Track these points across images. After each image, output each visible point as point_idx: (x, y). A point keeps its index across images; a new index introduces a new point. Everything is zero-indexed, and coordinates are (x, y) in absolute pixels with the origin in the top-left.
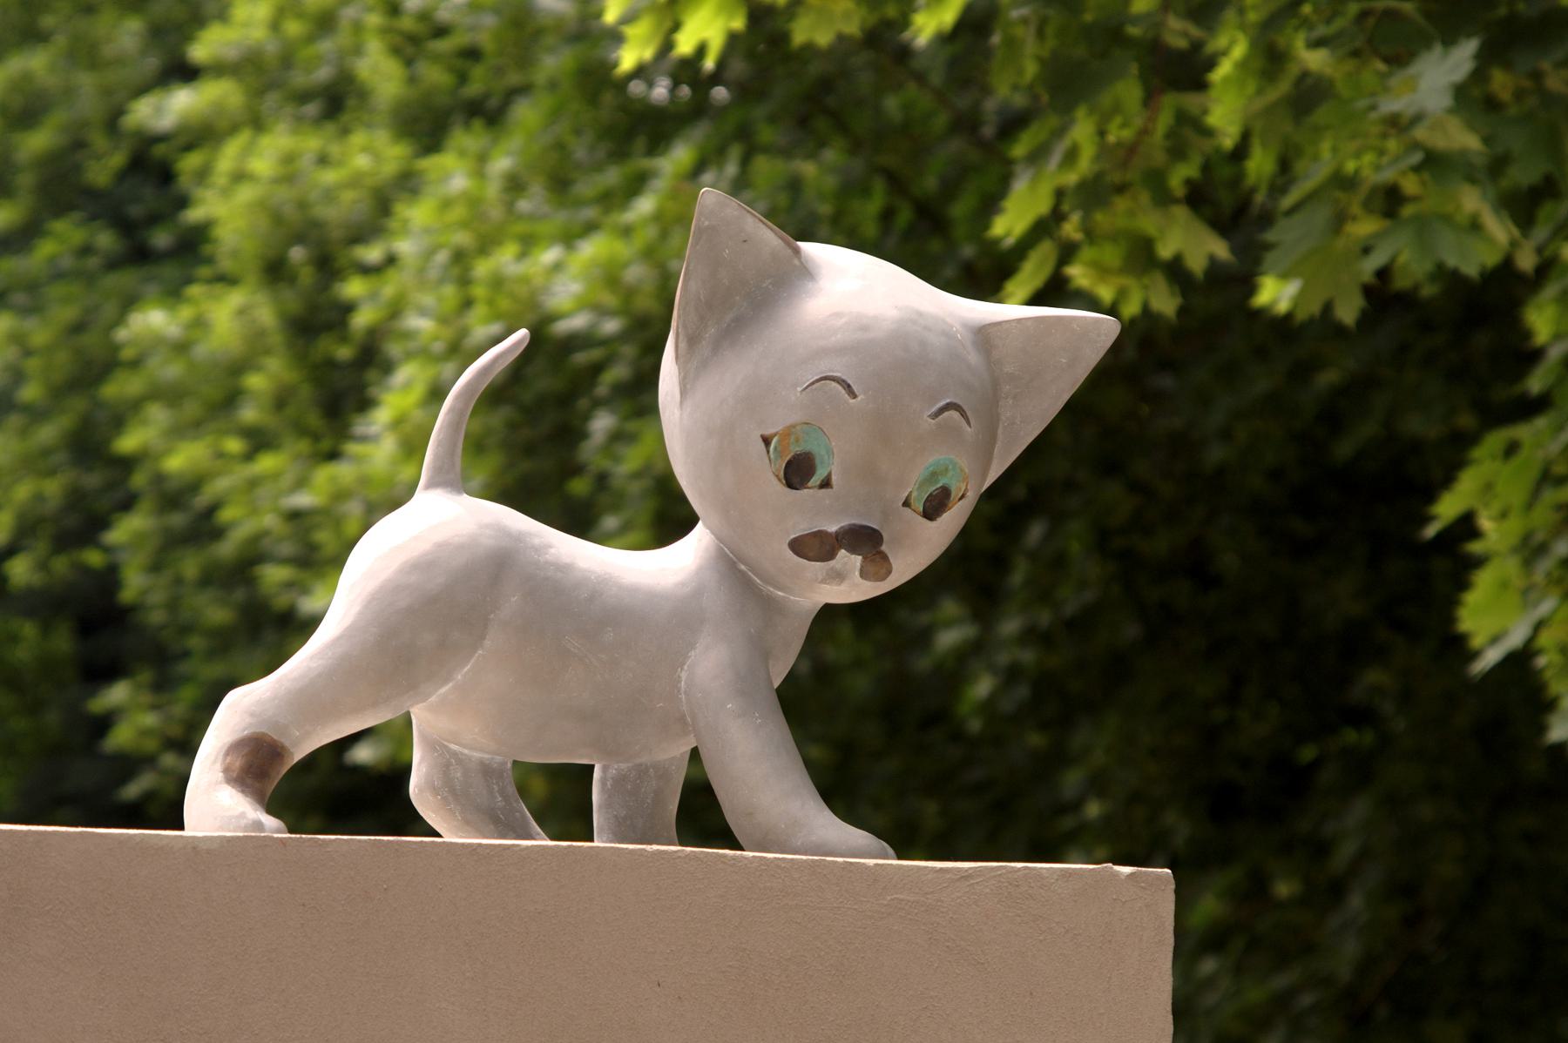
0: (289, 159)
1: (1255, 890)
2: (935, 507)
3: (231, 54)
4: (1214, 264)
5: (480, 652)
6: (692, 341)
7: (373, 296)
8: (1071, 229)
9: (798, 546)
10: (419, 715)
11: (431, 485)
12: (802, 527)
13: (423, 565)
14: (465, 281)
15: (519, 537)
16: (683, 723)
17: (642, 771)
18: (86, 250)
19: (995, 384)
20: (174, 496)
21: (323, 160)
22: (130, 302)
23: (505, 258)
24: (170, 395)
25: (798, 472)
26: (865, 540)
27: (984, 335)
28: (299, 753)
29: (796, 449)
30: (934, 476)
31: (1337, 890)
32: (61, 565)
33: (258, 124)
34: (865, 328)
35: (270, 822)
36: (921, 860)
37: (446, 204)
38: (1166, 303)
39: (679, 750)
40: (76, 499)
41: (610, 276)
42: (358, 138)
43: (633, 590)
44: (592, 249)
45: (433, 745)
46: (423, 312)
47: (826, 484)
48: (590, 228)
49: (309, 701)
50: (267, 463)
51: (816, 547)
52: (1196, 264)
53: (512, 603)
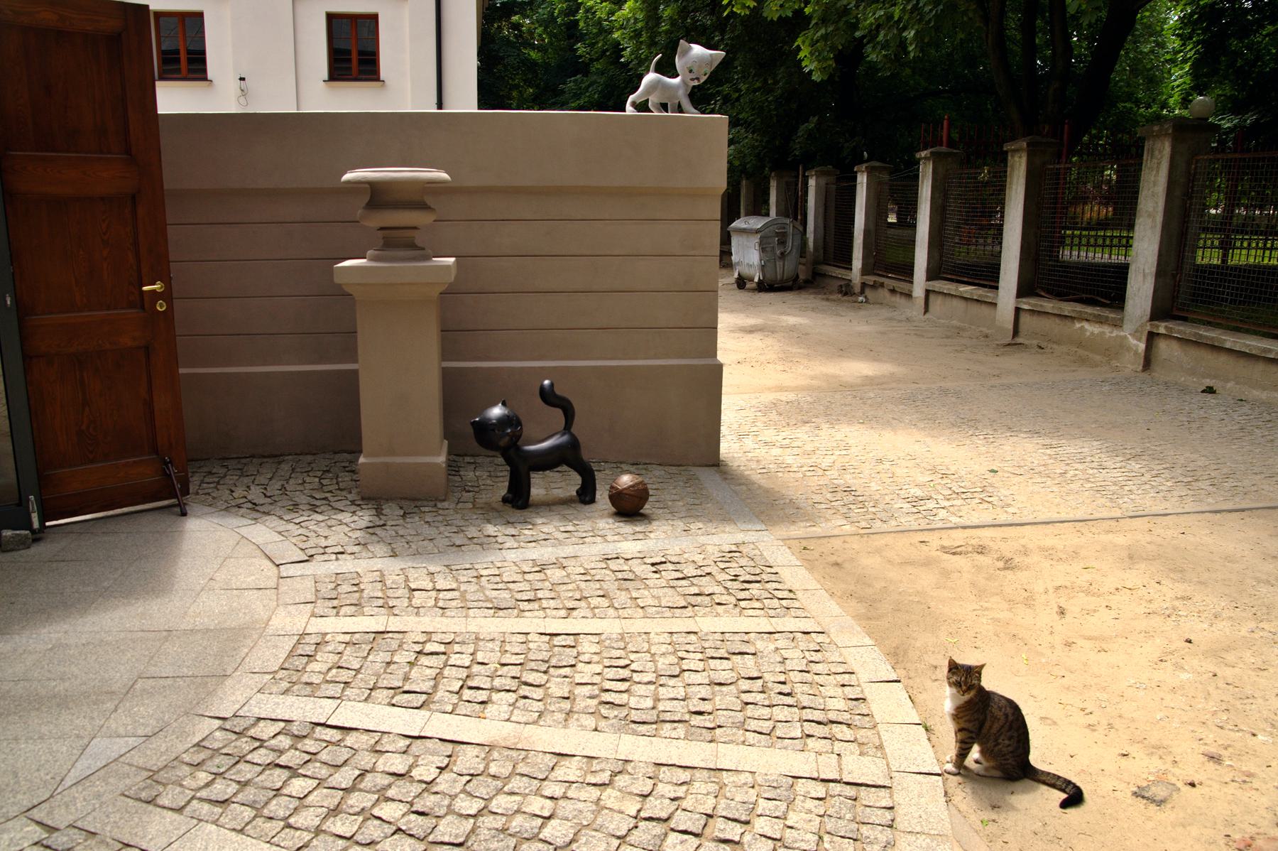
1: (765, 81)
4: (754, 6)
5: (921, 479)
6: (679, 57)
26: (698, 79)
27: (711, 55)
31: (778, 82)
36: (643, 366)
38: (748, 13)
39: (677, 101)
49: (639, 97)
51: (692, 80)
52: (752, 6)
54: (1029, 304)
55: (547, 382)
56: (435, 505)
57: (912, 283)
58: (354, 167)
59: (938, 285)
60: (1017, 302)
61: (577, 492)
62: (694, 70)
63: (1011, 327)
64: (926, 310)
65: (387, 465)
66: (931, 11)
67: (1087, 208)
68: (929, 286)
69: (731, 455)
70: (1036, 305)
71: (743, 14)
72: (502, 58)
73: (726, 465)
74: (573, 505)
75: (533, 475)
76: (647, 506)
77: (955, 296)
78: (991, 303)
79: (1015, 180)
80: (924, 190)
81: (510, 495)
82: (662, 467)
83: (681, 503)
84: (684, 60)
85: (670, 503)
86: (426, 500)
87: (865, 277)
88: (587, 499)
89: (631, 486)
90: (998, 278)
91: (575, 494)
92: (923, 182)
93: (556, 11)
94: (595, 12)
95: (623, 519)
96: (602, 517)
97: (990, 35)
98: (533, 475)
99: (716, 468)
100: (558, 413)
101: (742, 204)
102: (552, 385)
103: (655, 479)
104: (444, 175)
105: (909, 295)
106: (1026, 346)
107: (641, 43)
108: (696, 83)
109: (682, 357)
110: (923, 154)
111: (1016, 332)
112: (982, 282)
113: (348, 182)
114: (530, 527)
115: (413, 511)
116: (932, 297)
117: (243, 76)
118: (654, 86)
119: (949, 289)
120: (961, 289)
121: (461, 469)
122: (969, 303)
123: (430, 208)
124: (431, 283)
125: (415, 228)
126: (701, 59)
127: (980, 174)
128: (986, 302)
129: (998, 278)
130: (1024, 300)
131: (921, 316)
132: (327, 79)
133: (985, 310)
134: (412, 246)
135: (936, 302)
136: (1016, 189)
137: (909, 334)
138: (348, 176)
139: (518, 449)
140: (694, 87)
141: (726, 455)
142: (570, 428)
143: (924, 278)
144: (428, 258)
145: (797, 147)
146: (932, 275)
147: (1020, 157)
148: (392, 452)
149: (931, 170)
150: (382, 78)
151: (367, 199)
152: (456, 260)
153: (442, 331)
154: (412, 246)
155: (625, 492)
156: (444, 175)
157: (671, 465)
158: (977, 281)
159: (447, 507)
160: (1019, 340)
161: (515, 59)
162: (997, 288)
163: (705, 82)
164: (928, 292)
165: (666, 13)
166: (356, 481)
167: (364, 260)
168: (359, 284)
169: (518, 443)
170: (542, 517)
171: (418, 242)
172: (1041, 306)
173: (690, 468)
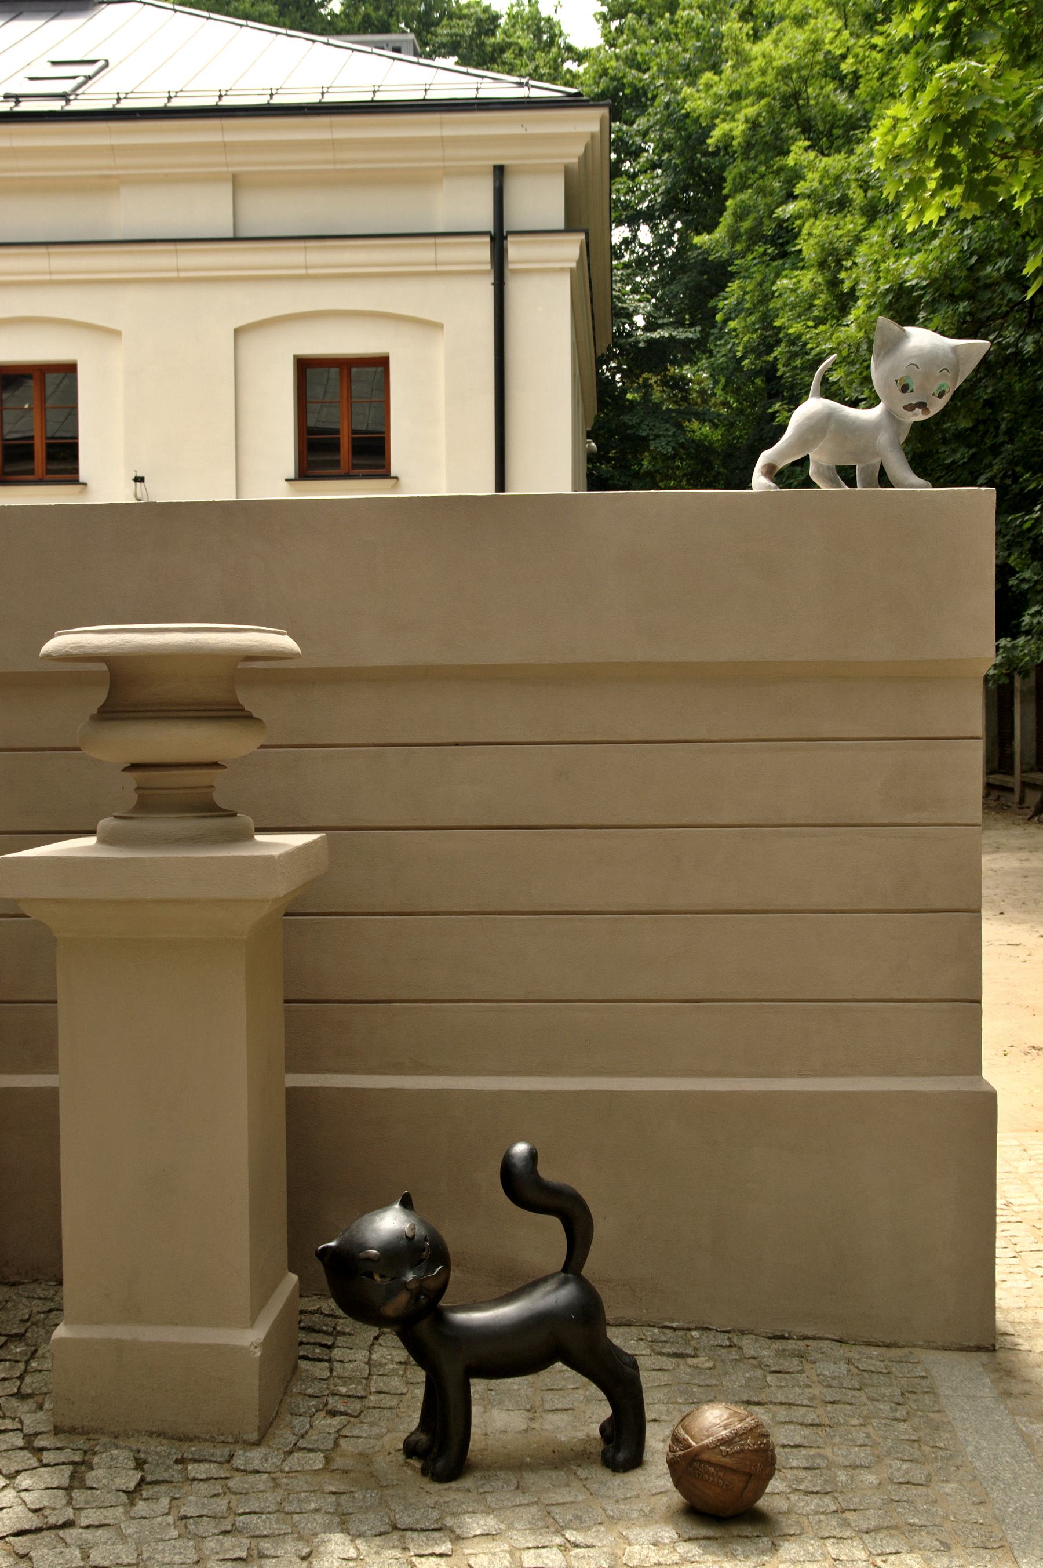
0: (826, 228)
2: (941, 395)
3: (808, 192)
6: (878, 356)
7: (849, 277)
9: (905, 408)
10: (811, 455)
11: (812, 396)
12: (906, 403)
13: (809, 418)
14: (878, 271)
15: (834, 409)
16: (878, 454)
17: (868, 466)
18: (765, 253)
19: (958, 361)
20: (793, 341)
21: (837, 227)
22: (778, 275)
23: (890, 263)
25: (905, 389)
26: (922, 405)
27: (955, 349)
28: (780, 467)
29: (903, 383)
30: (940, 387)
32: (924, 99)
33: (816, 215)
34: (922, 350)
35: (773, 485)
37: (872, 246)
39: (876, 461)
40: (763, 339)
41: (924, 267)
42: (849, 218)
43: (864, 421)
44: (919, 258)
45: (815, 462)
46: (864, 282)
47: (912, 391)
48: (919, 250)
49: (782, 454)
50: (821, 328)
51: (910, 408)
53: (832, 426)
55: (521, 1148)
61: (602, 1430)
62: (913, 386)
65: (119, 1347)
69: (1029, 1315)
72: (645, 440)
73: (1013, 1349)
74: (582, 1473)
75: (478, 1387)
76: (775, 1485)
81: (423, 1437)
82: (841, 1350)
83: (871, 1478)
84: (888, 364)
85: (842, 1477)
86: (212, 1440)
88: (621, 1456)
89: (724, 1442)
91: (597, 1433)
93: (740, 348)
95: (704, 1532)
96: (648, 1518)
98: (478, 1387)
99: (984, 1357)
100: (554, 1225)
101: (192, 855)
102: (533, 1156)
103: (816, 1390)
104: (285, 642)
108: (919, 416)
109: (892, 1072)
114: (445, 1547)
115: (166, 1476)
117: (139, 475)
118: (819, 427)
121: (341, 1340)
123: (249, 717)
124: (223, 900)
125: (215, 765)
126: (929, 360)
132: (292, 475)
138: (59, 643)
139: (439, 1317)
140: (917, 426)
141: (1016, 1316)
144: (243, 836)
145: (751, 156)
148: (133, 1314)
149: (106, 856)
150: (393, 473)
151: (100, 696)
152: (327, 835)
153: (286, 1002)
154: (209, 808)
155: (705, 1456)
156: (285, 642)
157: (869, 1344)
159: (256, 1464)
161: (668, 443)
163: (944, 413)
167: (91, 841)
168: (57, 901)
169: (442, 1304)
170: (489, 1511)
173: (919, 1354)
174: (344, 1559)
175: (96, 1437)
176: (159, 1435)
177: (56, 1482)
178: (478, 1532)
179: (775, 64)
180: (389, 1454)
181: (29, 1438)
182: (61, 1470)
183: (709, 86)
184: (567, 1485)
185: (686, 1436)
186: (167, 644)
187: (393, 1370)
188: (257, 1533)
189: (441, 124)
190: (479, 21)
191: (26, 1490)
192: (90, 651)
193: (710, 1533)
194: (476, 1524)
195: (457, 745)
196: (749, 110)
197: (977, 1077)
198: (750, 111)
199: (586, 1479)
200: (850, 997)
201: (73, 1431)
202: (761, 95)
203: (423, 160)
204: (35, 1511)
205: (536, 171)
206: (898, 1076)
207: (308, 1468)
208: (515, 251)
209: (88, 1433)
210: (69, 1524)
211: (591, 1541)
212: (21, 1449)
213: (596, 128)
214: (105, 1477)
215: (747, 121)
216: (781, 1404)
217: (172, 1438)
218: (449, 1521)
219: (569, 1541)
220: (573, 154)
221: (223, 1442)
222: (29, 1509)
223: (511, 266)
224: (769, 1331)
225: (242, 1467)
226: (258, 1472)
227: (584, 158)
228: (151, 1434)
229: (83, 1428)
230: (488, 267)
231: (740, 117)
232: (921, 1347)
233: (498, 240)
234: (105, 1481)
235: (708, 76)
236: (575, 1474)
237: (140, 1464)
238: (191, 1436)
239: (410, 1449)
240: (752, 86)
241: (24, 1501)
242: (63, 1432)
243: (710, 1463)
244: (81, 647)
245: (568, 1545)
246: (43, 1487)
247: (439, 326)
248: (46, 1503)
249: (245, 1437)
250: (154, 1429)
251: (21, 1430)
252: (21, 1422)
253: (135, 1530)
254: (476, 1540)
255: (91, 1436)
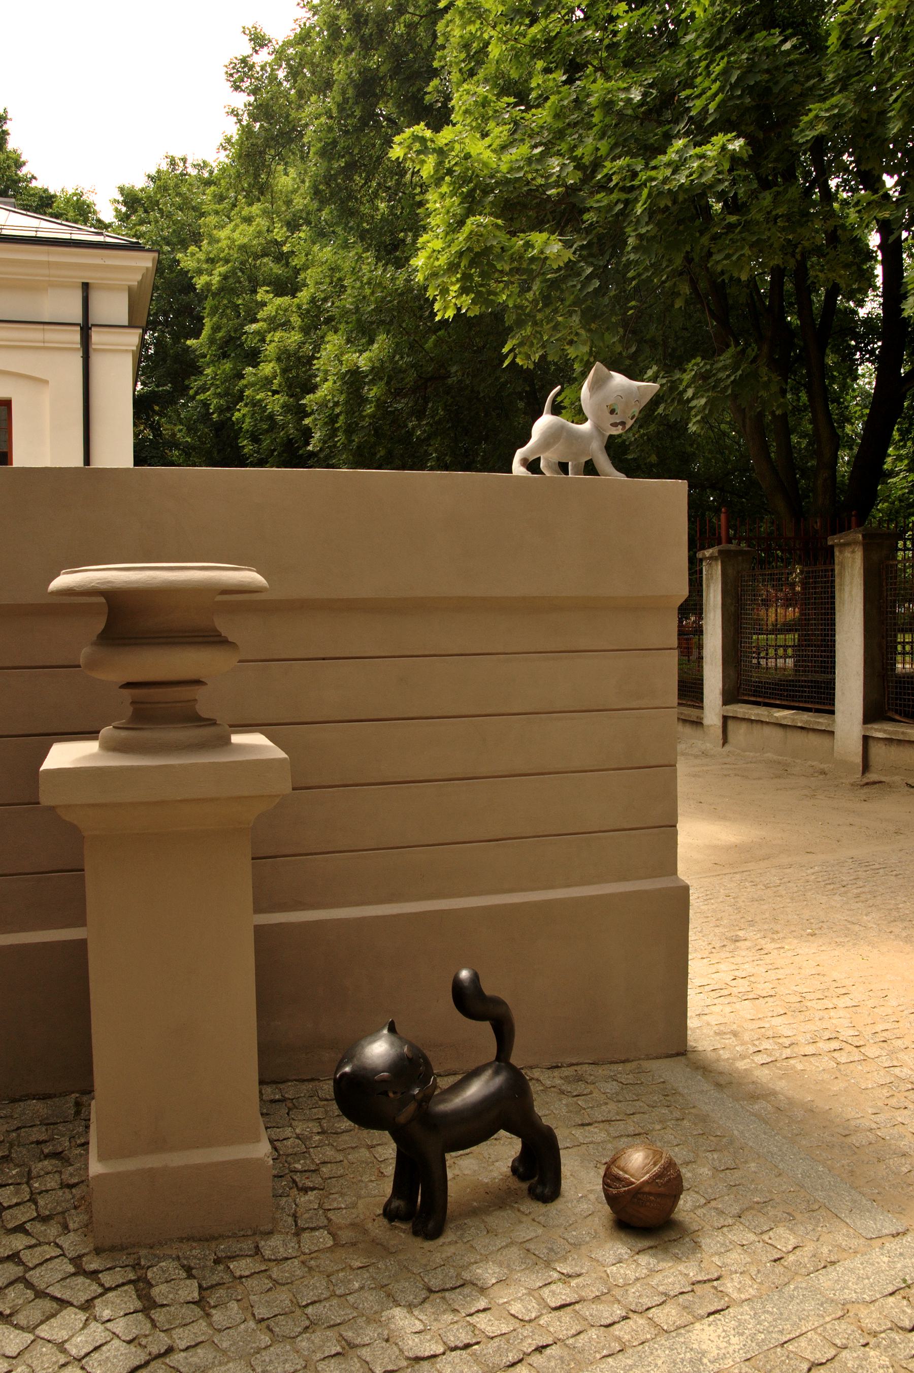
8: (517, 351)
9: (612, 425)
11: (547, 413)
12: (612, 422)
24: (253, 385)
44: (366, 355)
49: (532, 451)
51: (614, 425)
54: (885, 731)
55: (465, 974)
56: (257, 1250)
57: (702, 708)
58: (75, 563)
59: (740, 710)
60: (865, 729)
63: (858, 760)
64: (725, 741)
65: (151, 1174)
66: (729, 376)
67: (772, 611)
68: (727, 711)
70: (896, 732)
71: (525, 367)
75: (450, 1157)
77: (767, 723)
78: (828, 731)
79: (847, 579)
80: (712, 595)
87: (728, 707)
90: (834, 699)
92: (708, 586)
94: (266, 406)
95: (646, 1243)
97: (747, 421)
98: (450, 1157)
102: (475, 978)
104: (250, 576)
105: (698, 723)
106: (890, 785)
107: (337, 429)
109: (624, 879)
110: (708, 553)
111: (866, 766)
112: (801, 705)
113: (68, 592)
114: (482, 1304)
116: (731, 725)
119: (758, 715)
120: (777, 715)
122: (754, 724)
125: (198, 682)
127: (791, 574)
128: (814, 730)
129: (833, 695)
130: (876, 726)
131: (719, 749)
133: (814, 740)
134: (196, 719)
135: (739, 733)
136: (851, 592)
137: (729, 775)
138: (64, 580)
142: (508, 1055)
143: (719, 700)
146: (730, 696)
147: (853, 552)
148: (159, 1144)
151: (99, 625)
154: (196, 719)
157: (612, 1063)
158: (797, 704)
160: (872, 777)
162: (832, 712)
164: (725, 719)
165: (372, 394)
166: (71, 1186)
171: (204, 710)
172: (903, 733)
174: (416, 1333)
175: (135, 1250)
176: (188, 1240)
177: (132, 1307)
178: (494, 1281)
179: (236, 243)
180: (374, 1220)
181: (76, 1261)
182: (126, 1291)
183: (193, 254)
184: (520, 1222)
185: (627, 1176)
186: (189, 581)
187: (320, 1141)
188: (332, 1323)
189: (48, 253)
190: (41, 198)
191: (109, 1321)
192: (119, 586)
193: (652, 1243)
194: (488, 1273)
195: (324, 659)
196: (221, 269)
197: (673, 877)
198: (223, 269)
199: (530, 1213)
200: (597, 830)
201: (113, 1249)
202: (227, 261)
203: (36, 275)
204: (129, 1342)
205: (110, 288)
206: (628, 880)
207: (322, 1246)
208: (96, 337)
209: (127, 1248)
210: (170, 1350)
211: (577, 1269)
212: (74, 1274)
213: (149, 264)
214: (169, 1292)
215: (220, 275)
216: (603, 1121)
217: (201, 1240)
218: (466, 1275)
219: (563, 1274)
220: (134, 279)
221: (243, 1236)
222: (124, 1341)
223: (94, 347)
224: (548, 1064)
225: (273, 1257)
226: (287, 1259)
227: (140, 283)
228: (181, 1240)
229: (121, 1245)
230: (79, 346)
231: (216, 272)
232: (643, 1059)
233: (86, 329)
234: (171, 1296)
235: (192, 248)
236: (519, 1210)
237: (189, 1272)
238: (216, 1235)
239: (390, 1214)
240: (222, 255)
241: (114, 1333)
242: (105, 1251)
243: (650, 1194)
244: (109, 582)
245: (563, 1277)
246: (122, 1313)
247: (46, 382)
248: (137, 1332)
249: (262, 1229)
250: (184, 1236)
251: (63, 1255)
252: (61, 1247)
253: (229, 1343)
254: (495, 1288)
255: (130, 1251)
